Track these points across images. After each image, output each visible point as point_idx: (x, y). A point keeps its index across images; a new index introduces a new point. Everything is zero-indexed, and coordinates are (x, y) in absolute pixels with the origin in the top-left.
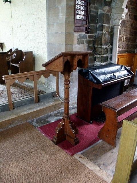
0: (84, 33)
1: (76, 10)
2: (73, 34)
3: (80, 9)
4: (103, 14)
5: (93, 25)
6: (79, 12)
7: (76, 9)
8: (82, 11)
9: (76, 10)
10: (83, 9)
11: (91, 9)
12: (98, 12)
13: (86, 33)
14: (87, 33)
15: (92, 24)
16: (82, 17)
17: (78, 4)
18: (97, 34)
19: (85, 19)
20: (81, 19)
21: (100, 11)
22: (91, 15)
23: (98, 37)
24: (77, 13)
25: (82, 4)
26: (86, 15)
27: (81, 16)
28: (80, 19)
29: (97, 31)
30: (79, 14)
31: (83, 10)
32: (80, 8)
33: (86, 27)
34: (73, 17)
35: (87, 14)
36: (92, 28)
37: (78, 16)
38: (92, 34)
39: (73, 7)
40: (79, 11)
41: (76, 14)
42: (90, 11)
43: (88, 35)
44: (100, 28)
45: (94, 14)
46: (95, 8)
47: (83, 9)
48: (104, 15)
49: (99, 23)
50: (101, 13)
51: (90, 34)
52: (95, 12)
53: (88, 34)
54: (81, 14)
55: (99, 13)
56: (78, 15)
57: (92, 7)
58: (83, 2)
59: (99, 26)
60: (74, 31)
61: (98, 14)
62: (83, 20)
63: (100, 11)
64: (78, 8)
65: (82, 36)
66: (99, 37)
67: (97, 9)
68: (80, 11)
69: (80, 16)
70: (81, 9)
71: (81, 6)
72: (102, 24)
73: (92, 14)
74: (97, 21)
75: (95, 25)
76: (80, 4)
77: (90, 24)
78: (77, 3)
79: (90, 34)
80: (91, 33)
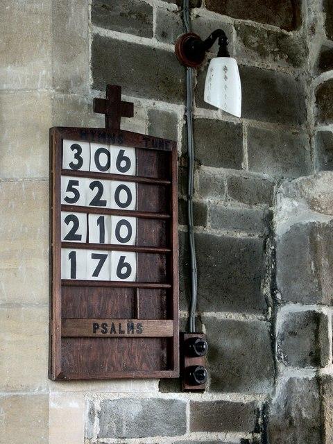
0: (150, 390)
1: (64, 215)
2: (47, 400)
3: (97, 207)
4: (313, 229)
5: (235, 316)
6: (89, 227)
7: (65, 208)
8: (116, 219)
9: (64, 215)
10: (103, 162)
11: (209, 200)
12: (270, 216)
13: (166, 384)
14: (182, 390)
15: (222, 316)
16: (122, 263)
17: (75, 171)
18: (279, 387)
19: (154, 275)
20: (115, 278)
21: (288, 213)
22: (207, 245)
23: (287, 415)
24: (72, 235)
25: (113, 170)
26: (156, 249)
27: (115, 256)
28: (103, 276)
29: (281, 367)
30: (94, 239)
31: (131, 242)
32: (97, 200)
33: (167, 342)
34: (43, 266)
35: (166, 240)
36: (229, 344)
37: (84, 256)
38: (233, 388)
39: (42, 194)
40: (94, 218)
41: (65, 246)
42: (200, 215)
43: (195, 406)
44: (292, 340)
45: (240, 235)
46: (236, 189)
47: (103, 162)
48: (319, 237)
49: (284, 303)
50: (296, 228)
51: (208, 397)
52: (244, 221)
53: (196, 397)
54: (115, 241)
55: (281, 225)
56: (87, 246)
57: (207, 186)
58: (121, 157)
59: (286, 325)
60: (50, 377)
61: (271, 233)
62: (133, 288)
63: (288, 213)
64: (84, 201)
65: (136, 410)
66: (293, 414)
67: (266, 195)
68: (72, 256)
69: (103, 258)
70: (112, 205)
71: (110, 187)
72: (314, 308)
73: (220, 233)
74: (274, 288)
75: (252, 318)
76: (94, 169)
77: (208, 315)
78: (66, 166)
79: (208, 397)
80: (218, 386)
